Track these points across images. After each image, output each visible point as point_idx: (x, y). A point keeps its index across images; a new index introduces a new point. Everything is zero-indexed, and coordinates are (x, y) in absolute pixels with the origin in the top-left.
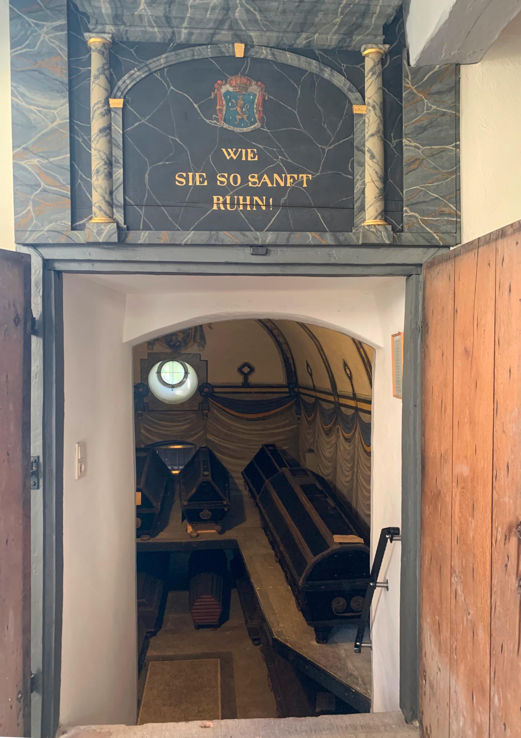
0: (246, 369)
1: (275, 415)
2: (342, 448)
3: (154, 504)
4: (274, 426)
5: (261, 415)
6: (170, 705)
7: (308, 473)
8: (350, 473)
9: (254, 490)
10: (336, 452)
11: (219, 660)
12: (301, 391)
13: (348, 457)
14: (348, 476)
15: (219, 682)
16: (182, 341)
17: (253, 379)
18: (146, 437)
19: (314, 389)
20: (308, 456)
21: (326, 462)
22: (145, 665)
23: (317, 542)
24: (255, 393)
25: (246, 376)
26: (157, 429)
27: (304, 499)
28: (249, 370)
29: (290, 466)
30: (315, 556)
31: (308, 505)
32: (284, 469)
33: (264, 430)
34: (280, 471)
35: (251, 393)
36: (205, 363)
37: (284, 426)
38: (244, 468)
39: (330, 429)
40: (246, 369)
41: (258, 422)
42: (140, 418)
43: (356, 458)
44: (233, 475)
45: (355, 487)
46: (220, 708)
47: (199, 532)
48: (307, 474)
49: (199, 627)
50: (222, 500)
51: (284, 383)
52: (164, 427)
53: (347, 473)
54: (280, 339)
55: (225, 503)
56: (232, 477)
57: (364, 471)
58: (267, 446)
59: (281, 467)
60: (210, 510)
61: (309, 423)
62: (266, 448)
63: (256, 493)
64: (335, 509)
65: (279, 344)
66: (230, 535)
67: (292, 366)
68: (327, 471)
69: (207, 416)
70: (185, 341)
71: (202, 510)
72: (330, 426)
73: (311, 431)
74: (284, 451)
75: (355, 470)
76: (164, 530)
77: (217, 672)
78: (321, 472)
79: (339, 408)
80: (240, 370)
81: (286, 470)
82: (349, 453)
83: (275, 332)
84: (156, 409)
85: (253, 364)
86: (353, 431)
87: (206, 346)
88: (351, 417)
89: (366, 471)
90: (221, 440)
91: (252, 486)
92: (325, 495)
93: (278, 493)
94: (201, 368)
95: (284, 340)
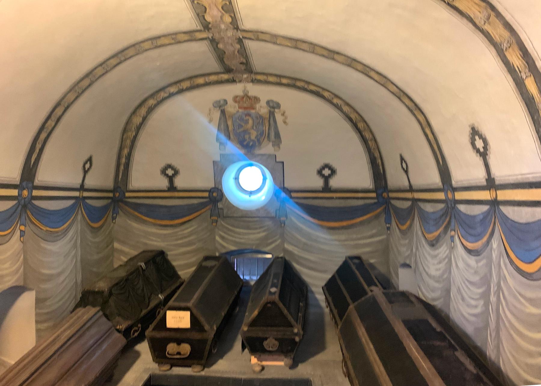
0: (327, 172)
1: (362, 223)
2: (461, 264)
3: (207, 327)
4: (359, 236)
5: (345, 223)
7: (413, 299)
8: (482, 302)
9: (335, 312)
12: (392, 195)
14: (476, 307)
16: (256, 140)
17: (334, 183)
18: (221, 244)
19: (411, 189)
20: (402, 272)
21: (432, 283)
25: (326, 179)
26: (233, 236)
28: (330, 172)
32: (373, 288)
34: (370, 294)
35: (332, 198)
36: (281, 165)
40: (327, 172)
44: (314, 289)
47: (264, 363)
48: (412, 302)
50: (292, 326)
53: (473, 303)
54: (367, 135)
55: (296, 331)
56: (312, 292)
57: (518, 306)
58: (352, 258)
59: (369, 285)
60: (276, 339)
65: (364, 140)
66: (304, 370)
67: (381, 167)
70: (258, 140)
71: (266, 339)
72: (436, 234)
73: (407, 241)
74: (371, 265)
75: (493, 299)
76: (224, 358)
78: (423, 293)
79: (454, 208)
80: (320, 172)
81: (377, 292)
83: (361, 125)
85: (334, 165)
86: (485, 239)
87: (281, 146)
88: (481, 217)
89: (525, 306)
93: (368, 330)
94: (277, 168)
95: (371, 136)
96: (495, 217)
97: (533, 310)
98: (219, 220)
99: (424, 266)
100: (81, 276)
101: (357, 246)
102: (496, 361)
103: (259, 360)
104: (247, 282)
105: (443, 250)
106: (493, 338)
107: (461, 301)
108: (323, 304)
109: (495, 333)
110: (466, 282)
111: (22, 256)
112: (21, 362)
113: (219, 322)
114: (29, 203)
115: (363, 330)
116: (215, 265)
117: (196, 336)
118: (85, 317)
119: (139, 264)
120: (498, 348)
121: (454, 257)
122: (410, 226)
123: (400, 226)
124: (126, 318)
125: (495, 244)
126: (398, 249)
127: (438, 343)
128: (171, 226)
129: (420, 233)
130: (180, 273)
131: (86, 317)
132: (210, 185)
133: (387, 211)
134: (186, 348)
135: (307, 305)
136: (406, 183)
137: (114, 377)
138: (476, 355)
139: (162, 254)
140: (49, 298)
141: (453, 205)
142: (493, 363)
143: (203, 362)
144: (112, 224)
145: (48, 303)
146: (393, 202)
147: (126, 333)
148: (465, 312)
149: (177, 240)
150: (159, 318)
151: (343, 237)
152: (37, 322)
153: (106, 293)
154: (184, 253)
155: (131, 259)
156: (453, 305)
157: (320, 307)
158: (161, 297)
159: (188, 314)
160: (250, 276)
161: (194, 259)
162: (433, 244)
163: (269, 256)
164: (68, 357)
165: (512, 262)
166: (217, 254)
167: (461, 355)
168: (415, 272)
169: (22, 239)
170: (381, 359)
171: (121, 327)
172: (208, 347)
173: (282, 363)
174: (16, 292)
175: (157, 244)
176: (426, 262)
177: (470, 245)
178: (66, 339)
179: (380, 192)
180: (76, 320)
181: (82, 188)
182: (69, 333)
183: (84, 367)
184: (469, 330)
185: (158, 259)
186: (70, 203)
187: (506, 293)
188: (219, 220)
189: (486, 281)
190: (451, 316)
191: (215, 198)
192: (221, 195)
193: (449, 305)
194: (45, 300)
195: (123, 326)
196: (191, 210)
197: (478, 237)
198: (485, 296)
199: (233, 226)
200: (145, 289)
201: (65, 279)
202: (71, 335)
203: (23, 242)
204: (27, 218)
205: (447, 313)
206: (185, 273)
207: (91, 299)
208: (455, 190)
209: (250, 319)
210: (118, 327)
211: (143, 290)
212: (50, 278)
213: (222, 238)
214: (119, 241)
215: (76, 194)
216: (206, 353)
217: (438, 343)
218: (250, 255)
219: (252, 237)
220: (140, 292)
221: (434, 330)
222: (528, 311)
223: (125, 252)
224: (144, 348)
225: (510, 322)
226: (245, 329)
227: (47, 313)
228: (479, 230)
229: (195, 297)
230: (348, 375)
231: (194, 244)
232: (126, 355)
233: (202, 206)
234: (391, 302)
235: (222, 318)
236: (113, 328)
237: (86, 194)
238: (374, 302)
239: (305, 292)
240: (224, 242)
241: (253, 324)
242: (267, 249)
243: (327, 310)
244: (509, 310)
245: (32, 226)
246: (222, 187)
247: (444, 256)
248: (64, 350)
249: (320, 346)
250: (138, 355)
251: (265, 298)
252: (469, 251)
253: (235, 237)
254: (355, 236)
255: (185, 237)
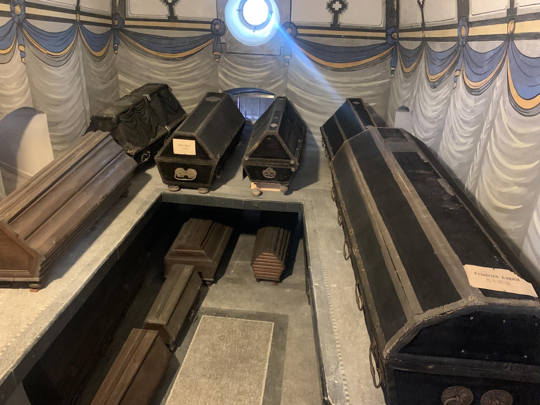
1: (366, 65)
2: (459, 105)
3: (211, 156)
4: (362, 79)
5: (349, 65)
6: (210, 378)
7: (406, 135)
8: (471, 140)
9: (330, 148)
10: (446, 111)
11: (273, 323)
13: (471, 118)
14: (465, 144)
15: (268, 354)
17: (345, 19)
18: (224, 82)
21: (427, 124)
22: (197, 319)
23: (435, 284)
24: (346, 37)
25: (336, 14)
26: (236, 74)
27: (399, 175)
28: (340, 6)
29: (378, 126)
30: (425, 310)
31: (408, 189)
32: (369, 127)
33: (350, 83)
35: (340, 37)
37: (375, 79)
38: (323, 123)
39: (440, 81)
41: (345, 73)
42: (217, 60)
43: (490, 117)
44: (312, 130)
45: (477, 160)
46: (263, 392)
47: (262, 189)
48: (404, 138)
49: (259, 280)
51: (382, 26)
52: (242, 72)
53: (463, 140)
55: (292, 162)
56: (310, 132)
57: (506, 141)
58: (352, 100)
60: (274, 169)
61: (407, 76)
62: (350, 103)
63: (332, 153)
64: (454, 200)
66: (297, 196)
68: (425, 135)
69: (288, 63)
71: (265, 168)
72: (440, 74)
74: (370, 108)
75: (483, 136)
76: (227, 184)
77: (268, 341)
81: (373, 130)
82: (472, 112)
84: (234, 51)
88: (491, 54)
90: (302, 91)
91: (329, 145)
92: (435, 172)
96: (506, 53)
97: (520, 144)
98: (222, 55)
99: (422, 108)
100: (89, 105)
101: (358, 89)
102: (472, 191)
103: (259, 186)
104: (249, 121)
105: (444, 91)
106: (473, 173)
107: (451, 139)
108: (320, 143)
109: (477, 167)
110: (461, 122)
111: (27, 78)
112: (42, 173)
113: (223, 152)
114: (24, 21)
115: (355, 160)
116: (219, 101)
117: (201, 162)
118: (96, 140)
119: (144, 95)
120: (476, 180)
121: (454, 97)
122: (414, 70)
123: (404, 69)
124: (136, 145)
125: (499, 82)
126: (398, 92)
127: (422, 172)
128: (174, 60)
129: (424, 75)
130: (184, 108)
131: (97, 140)
132: (212, 15)
133: (393, 54)
134: (192, 173)
135: (304, 143)
136: (420, 21)
137: (129, 194)
138: (457, 185)
139: (165, 87)
140: (62, 122)
141: (464, 43)
142: (469, 193)
143: (208, 185)
144: (115, 55)
145: (60, 127)
146: (401, 42)
147: (137, 157)
148: (451, 151)
149: (180, 74)
150: (166, 144)
151: (346, 79)
152: (53, 143)
153: (114, 120)
154: (189, 89)
155: (136, 91)
156: (443, 143)
157: (317, 147)
158: (168, 128)
159: (194, 142)
160: (252, 115)
161: (197, 96)
162: (434, 86)
163: (272, 97)
164: (85, 172)
165: (511, 98)
166: (220, 92)
167: (442, 182)
168: (412, 114)
169: (23, 59)
170: (369, 184)
171: (131, 152)
172: (212, 173)
173: (279, 190)
174: (27, 113)
175: (161, 78)
176: (425, 104)
177: (472, 85)
178: (81, 157)
179: (390, 31)
180: (88, 142)
181: (78, 11)
182: (82, 152)
183: (101, 181)
184: (453, 165)
185: (162, 92)
186: (67, 26)
187: (498, 130)
188: (222, 55)
189: (480, 120)
190: (438, 154)
191: (218, 31)
192: (224, 28)
193: (439, 144)
194: (57, 123)
195: (133, 151)
196: (194, 43)
197: (482, 76)
198: (476, 135)
199: (235, 63)
200: (151, 119)
201: (74, 106)
202: (84, 154)
203: (25, 64)
204: (25, 39)
205: (436, 151)
206: (189, 109)
207: (100, 124)
208: (470, 24)
209: (251, 150)
210: (128, 152)
211: (150, 121)
212: (58, 103)
213: (225, 75)
214: (124, 74)
215: (73, 17)
216: (211, 178)
217: (422, 172)
218: (252, 95)
219: (255, 75)
220: (146, 121)
221: (422, 161)
222: (514, 145)
223: (130, 84)
224: (154, 172)
225: (494, 157)
226: (247, 158)
227: (62, 136)
228: (486, 68)
229: (200, 127)
230: (336, 200)
231: (197, 80)
232: (138, 174)
233: (205, 39)
234: (384, 137)
235: (225, 149)
236: (124, 151)
237: (83, 18)
238: (369, 136)
239: (304, 131)
240: (227, 81)
241: (254, 155)
242: (269, 89)
243: (323, 149)
244: (497, 146)
245: (31, 47)
246: (224, 19)
247: (444, 97)
248: (80, 166)
249: (313, 177)
250: (149, 178)
251: (266, 132)
252: (470, 91)
253: (238, 75)
254: (358, 79)
255: (189, 72)
